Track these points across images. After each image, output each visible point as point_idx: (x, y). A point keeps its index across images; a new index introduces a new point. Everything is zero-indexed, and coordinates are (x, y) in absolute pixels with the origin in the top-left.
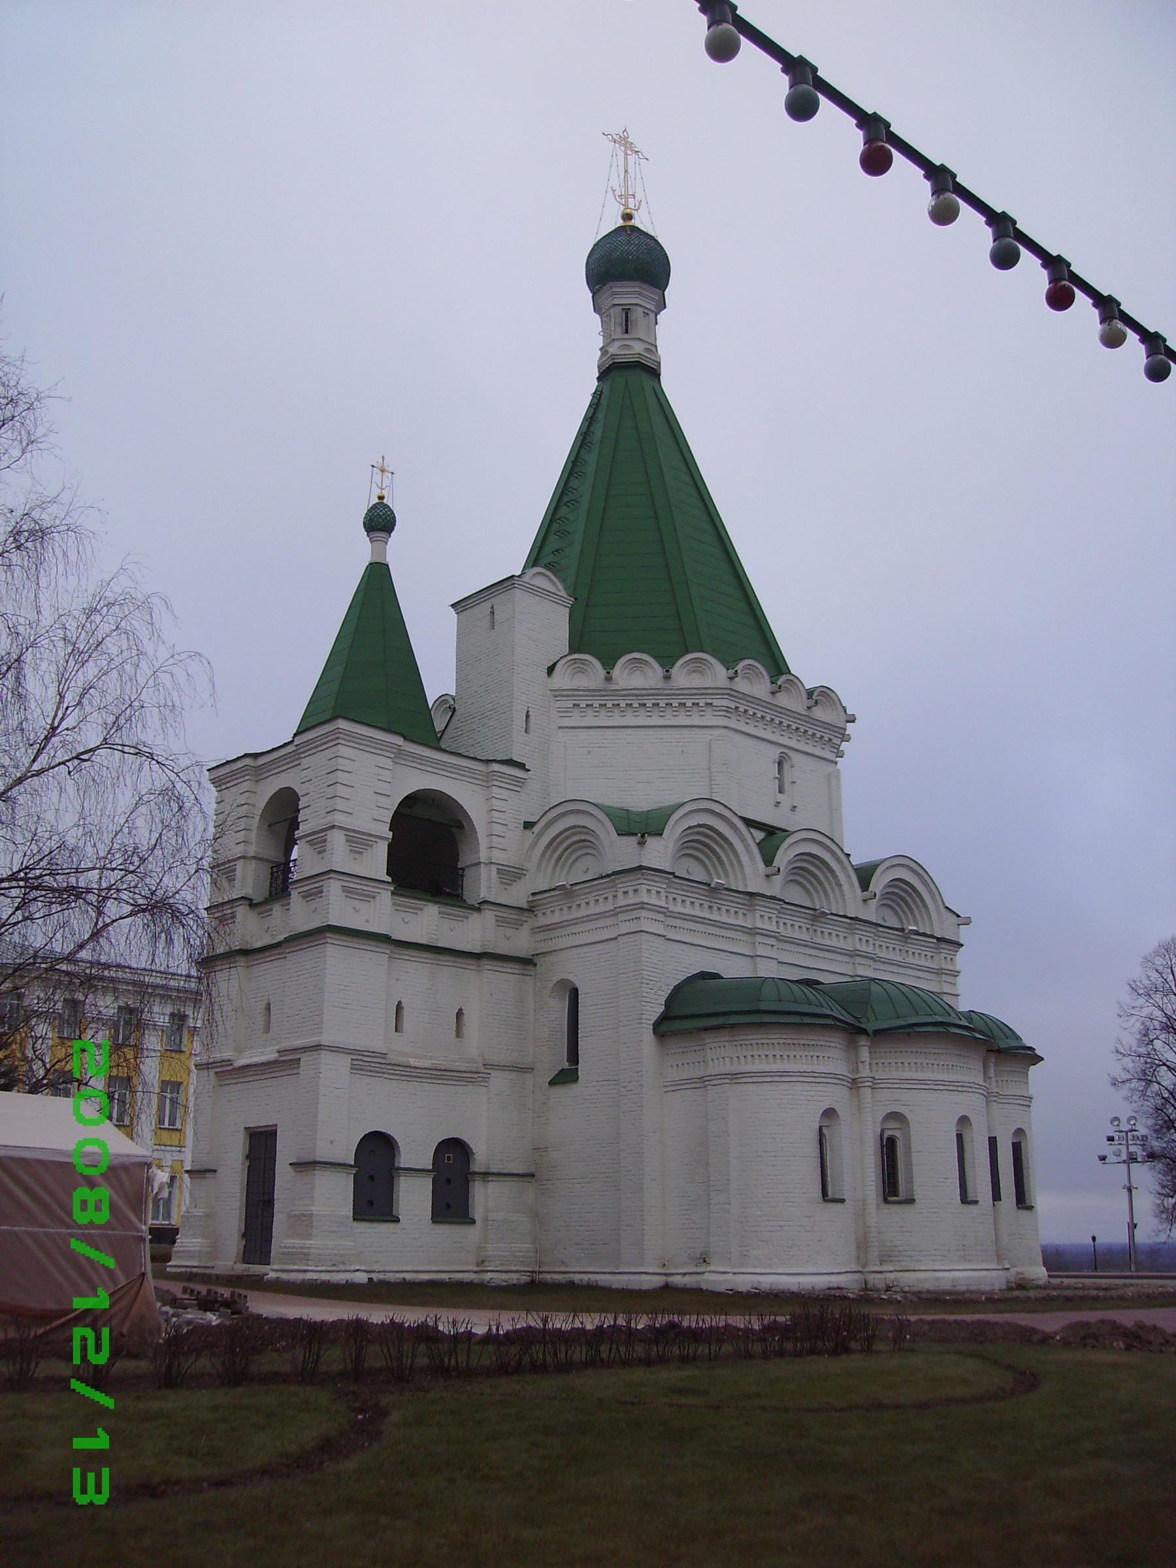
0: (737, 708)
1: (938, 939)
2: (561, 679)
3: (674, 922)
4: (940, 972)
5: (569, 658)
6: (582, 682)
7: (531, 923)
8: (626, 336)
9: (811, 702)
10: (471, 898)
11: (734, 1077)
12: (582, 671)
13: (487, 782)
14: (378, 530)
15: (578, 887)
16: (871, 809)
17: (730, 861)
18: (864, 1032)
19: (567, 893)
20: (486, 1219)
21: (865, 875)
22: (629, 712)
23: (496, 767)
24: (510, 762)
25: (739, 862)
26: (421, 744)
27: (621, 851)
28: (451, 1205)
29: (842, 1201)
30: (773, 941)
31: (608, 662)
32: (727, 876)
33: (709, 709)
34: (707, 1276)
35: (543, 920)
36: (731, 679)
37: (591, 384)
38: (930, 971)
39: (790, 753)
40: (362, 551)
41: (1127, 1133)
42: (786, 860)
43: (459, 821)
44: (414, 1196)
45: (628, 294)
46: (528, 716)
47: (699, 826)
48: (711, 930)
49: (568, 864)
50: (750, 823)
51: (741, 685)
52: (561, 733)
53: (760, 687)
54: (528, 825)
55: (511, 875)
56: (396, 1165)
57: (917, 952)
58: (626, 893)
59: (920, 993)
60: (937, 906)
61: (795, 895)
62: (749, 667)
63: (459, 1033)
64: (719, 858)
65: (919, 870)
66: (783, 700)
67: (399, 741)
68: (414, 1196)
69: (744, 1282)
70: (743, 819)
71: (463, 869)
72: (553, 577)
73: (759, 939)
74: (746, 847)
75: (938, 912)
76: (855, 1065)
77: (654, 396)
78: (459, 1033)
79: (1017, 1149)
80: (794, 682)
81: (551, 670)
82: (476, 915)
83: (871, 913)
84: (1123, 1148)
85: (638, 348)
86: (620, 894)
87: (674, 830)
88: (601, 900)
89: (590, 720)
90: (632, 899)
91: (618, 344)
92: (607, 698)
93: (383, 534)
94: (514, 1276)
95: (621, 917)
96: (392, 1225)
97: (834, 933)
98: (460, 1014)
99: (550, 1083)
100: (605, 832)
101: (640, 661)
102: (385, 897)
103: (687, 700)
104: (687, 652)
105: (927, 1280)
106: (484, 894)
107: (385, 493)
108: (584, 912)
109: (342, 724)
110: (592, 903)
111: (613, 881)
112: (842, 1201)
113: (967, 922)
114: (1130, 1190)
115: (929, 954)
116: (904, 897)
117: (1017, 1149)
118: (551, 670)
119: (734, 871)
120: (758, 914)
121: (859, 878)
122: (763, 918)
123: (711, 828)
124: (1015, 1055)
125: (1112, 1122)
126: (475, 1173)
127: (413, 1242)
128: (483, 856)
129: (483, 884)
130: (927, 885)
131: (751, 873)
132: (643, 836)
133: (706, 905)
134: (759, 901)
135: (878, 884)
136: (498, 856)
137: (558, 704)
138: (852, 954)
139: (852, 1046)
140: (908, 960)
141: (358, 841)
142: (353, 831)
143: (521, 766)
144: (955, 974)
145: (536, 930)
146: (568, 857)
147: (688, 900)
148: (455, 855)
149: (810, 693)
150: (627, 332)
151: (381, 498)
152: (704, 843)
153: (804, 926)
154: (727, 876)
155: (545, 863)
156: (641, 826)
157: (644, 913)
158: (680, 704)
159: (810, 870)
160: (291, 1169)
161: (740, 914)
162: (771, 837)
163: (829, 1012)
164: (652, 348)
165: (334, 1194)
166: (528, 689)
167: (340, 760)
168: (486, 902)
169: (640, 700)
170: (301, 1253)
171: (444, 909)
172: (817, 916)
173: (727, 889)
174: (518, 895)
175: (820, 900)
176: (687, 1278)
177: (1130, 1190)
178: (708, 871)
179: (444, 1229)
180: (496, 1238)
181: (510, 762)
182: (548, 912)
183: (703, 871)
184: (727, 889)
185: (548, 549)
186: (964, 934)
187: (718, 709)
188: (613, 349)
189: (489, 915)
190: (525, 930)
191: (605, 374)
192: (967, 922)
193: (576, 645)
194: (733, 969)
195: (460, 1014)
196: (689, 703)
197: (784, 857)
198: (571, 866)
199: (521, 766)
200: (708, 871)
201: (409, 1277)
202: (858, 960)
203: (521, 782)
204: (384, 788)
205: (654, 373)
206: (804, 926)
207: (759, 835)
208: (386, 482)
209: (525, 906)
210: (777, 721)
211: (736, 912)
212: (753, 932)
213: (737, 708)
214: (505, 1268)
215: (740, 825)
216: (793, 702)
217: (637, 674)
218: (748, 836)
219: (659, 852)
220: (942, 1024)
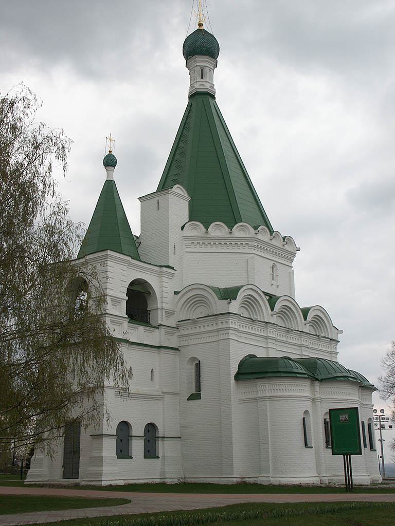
0: (258, 245)
1: (331, 339)
2: (188, 232)
3: (239, 334)
4: (331, 353)
5: (190, 223)
6: (194, 233)
7: (178, 334)
8: (202, 80)
9: (285, 243)
10: (153, 323)
11: (270, 397)
12: (195, 228)
13: (160, 275)
14: (110, 166)
15: (200, 319)
16: (308, 285)
17: (258, 309)
18: (317, 380)
19: (195, 322)
20: (164, 457)
21: (305, 312)
22: (214, 246)
23: (164, 269)
24: (168, 267)
25: (262, 309)
26: (114, 251)
27: (220, 306)
28: (150, 452)
29: (312, 447)
30: (274, 341)
31: (231, 227)
32: (257, 315)
33: (246, 246)
34: (260, 478)
35: (182, 332)
36: (256, 234)
37: (185, 101)
38: (328, 352)
39: (277, 264)
40: (102, 175)
41: (380, 416)
42: (278, 308)
43: (149, 292)
44: (137, 447)
45: (202, 61)
46: (174, 247)
47: (249, 295)
48: (253, 337)
49: (193, 309)
50: (266, 294)
51: (260, 236)
52: (186, 254)
53: (265, 237)
54: (176, 293)
55: (170, 313)
56: (130, 434)
57: (314, 343)
58: (222, 323)
59: (330, 363)
60: (330, 326)
61: (280, 323)
62: (262, 229)
63: (152, 379)
64: (254, 308)
65: (320, 309)
66: (274, 242)
67: (130, 259)
68: (137, 447)
69: (296, 481)
70: (263, 292)
71: (150, 311)
72: (183, 189)
73: (269, 340)
74: (264, 303)
75: (331, 328)
76: (313, 392)
77: (216, 113)
78: (152, 379)
79: (369, 425)
80: (278, 234)
81: (183, 228)
82: (157, 330)
83: (307, 329)
84: (378, 423)
85: (208, 86)
86: (219, 323)
87: (241, 295)
88: (210, 325)
89: (198, 249)
90: (225, 326)
91: (199, 83)
92: (206, 240)
93: (113, 168)
94: (235, 480)
95: (220, 332)
96: (130, 460)
97: (259, 329)
98: (152, 371)
99: (188, 399)
100: (213, 298)
101: (222, 226)
102: (126, 323)
103: (237, 242)
104: (236, 223)
105: (214, 481)
106: (160, 322)
107: (112, 149)
108: (203, 330)
109: (109, 252)
110: (206, 326)
111: (217, 317)
112: (312, 447)
113: (341, 332)
114: (381, 442)
115: (327, 345)
116: (317, 322)
117: (369, 425)
118: (183, 228)
119: (288, 322)
120: (303, 339)
121: (303, 315)
122: (271, 333)
123: (290, 308)
124: (368, 388)
125: (380, 411)
126: (132, 436)
127: (138, 469)
128: (159, 306)
129: (160, 318)
130: (326, 317)
131: (266, 314)
132: (231, 300)
133: (251, 327)
134: (269, 325)
135: (310, 316)
136: (165, 306)
137: (185, 242)
138: (301, 346)
139: (312, 385)
140: (320, 348)
141: (116, 301)
142: (114, 297)
143: (172, 268)
144: (337, 353)
145: (180, 337)
146: (195, 305)
147: (248, 326)
148: (145, 304)
149: (284, 238)
150: (202, 78)
151: (110, 152)
152: (250, 302)
153: (284, 335)
154: (257, 315)
155: (189, 311)
156: (229, 294)
157: (231, 331)
158: (235, 244)
159: (287, 312)
160: (91, 437)
161: (262, 331)
162: (272, 300)
163: (305, 372)
164: (212, 86)
165: (109, 448)
166: (174, 236)
167: (108, 267)
168: (161, 325)
169: (219, 241)
170: (98, 473)
171: (146, 328)
172: (289, 331)
173: (258, 321)
174: (172, 322)
175: (319, 331)
176: (251, 479)
177: (381, 442)
178: (285, 322)
179: (146, 459)
180: (168, 466)
181: (168, 267)
182: (185, 329)
183: (283, 322)
184: (258, 321)
185: (171, 173)
186: (340, 337)
187: (251, 246)
188: (197, 86)
189: (163, 330)
190: (175, 337)
191: (192, 97)
192: (341, 332)
193: (192, 218)
194: (261, 354)
195: (152, 371)
196: (233, 243)
197: (277, 307)
198: (195, 310)
199: (172, 268)
200: (285, 322)
201: (137, 482)
202: (303, 348)
203: (173, 275)
204: (124, 278)
205: (213, 97)
206: (284, 335)
207: (268, 298)
208: (112, 145)
209: (175, 326)
210: (278, 253)
211: (261, 330)
212: (266, 338)
213: (258, 245)
214: (90, 479)
215: (262, 295)
216: (278, 243)
217: (218, 230)
218: (264, 298)
219: (235, 306)
220: (346, 376)
